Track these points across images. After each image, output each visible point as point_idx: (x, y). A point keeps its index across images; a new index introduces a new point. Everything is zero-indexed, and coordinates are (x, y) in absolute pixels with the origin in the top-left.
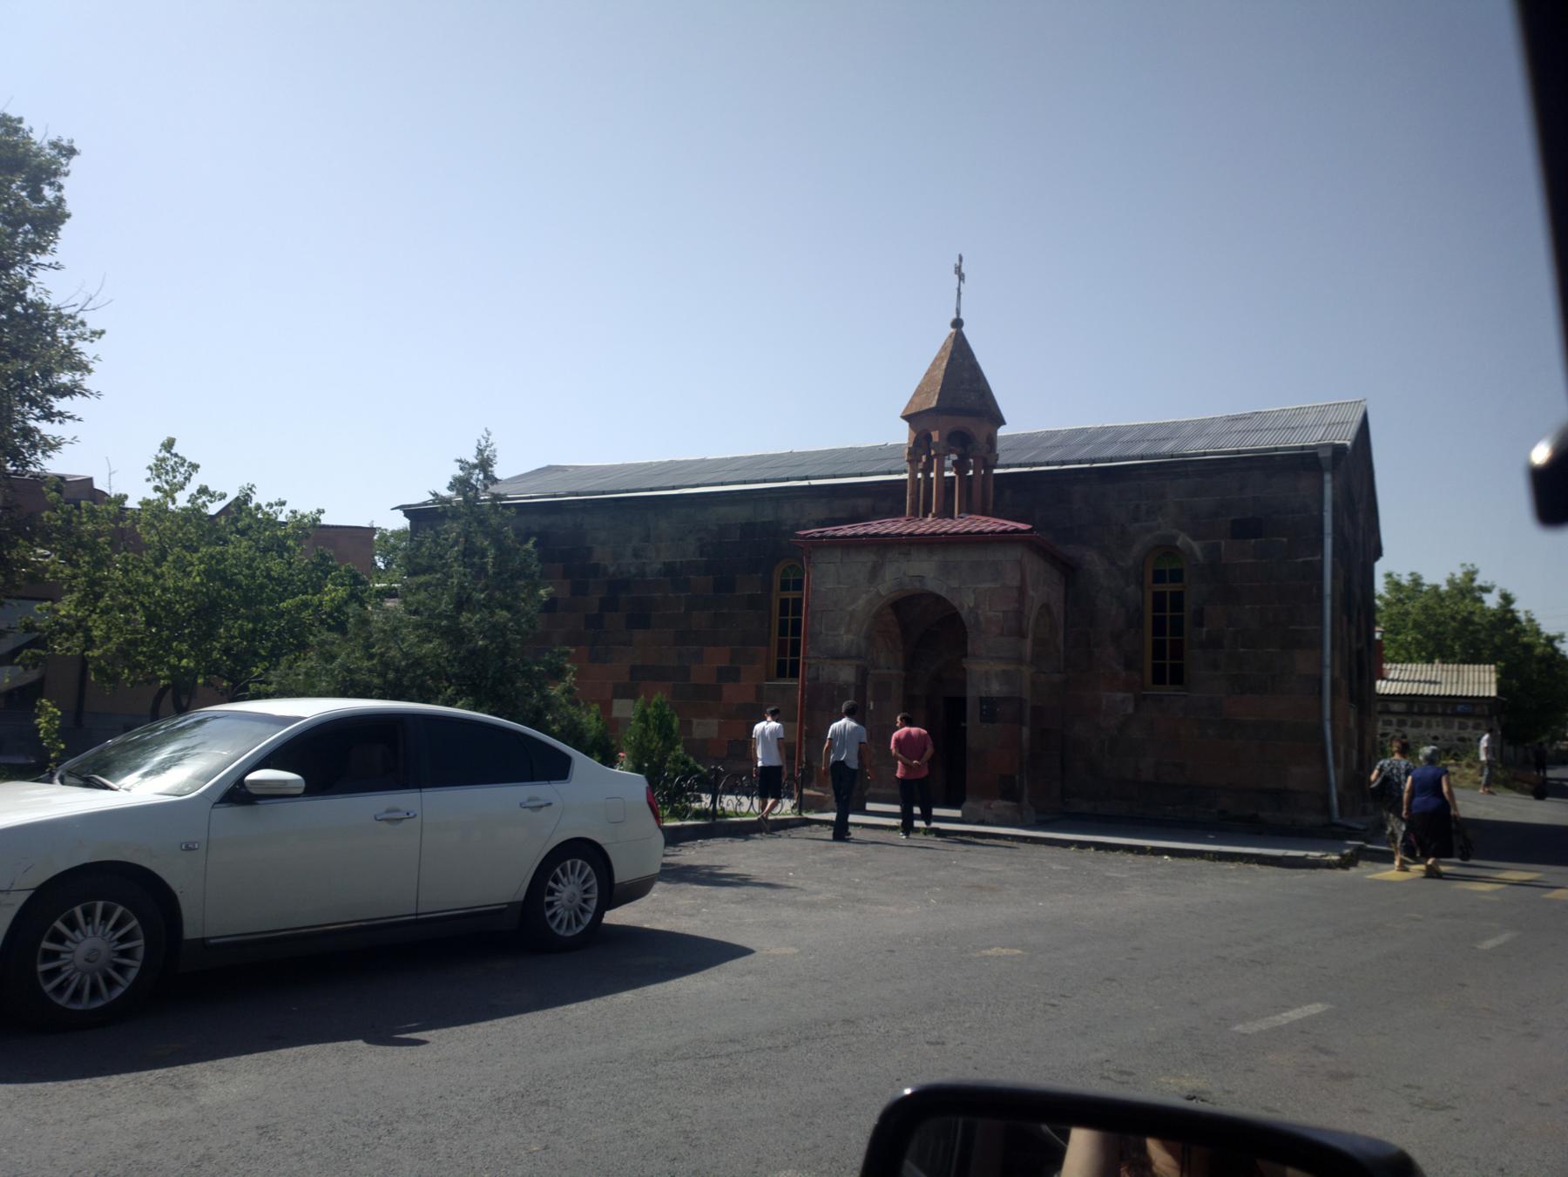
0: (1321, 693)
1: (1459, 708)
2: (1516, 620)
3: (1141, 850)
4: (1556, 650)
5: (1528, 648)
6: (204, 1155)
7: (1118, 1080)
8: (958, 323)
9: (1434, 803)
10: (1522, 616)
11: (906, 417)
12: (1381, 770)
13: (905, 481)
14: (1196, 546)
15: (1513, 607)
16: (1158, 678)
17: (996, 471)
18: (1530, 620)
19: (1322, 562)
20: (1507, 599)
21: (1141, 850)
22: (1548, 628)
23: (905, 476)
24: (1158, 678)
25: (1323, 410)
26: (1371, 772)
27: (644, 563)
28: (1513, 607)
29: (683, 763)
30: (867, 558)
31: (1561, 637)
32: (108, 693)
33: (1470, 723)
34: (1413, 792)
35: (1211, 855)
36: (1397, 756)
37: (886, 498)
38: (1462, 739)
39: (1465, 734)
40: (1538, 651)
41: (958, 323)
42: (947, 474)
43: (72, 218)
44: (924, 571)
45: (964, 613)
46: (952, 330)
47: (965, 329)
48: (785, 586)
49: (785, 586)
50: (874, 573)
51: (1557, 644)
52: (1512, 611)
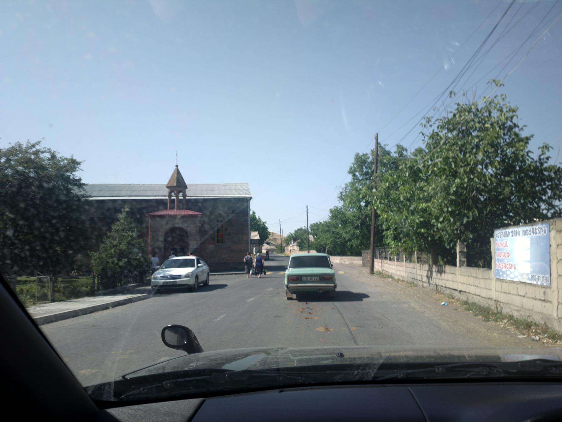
0: (248, 243)
1: (252, 242)
2: (256, 218)
3: (229, 274)
4: (265, 225)
6: (430, 214)
8: (177, 166)
10: (257, 217)
12: (246, 259)
13: (167, 199)
16: (218, 241)
17: (187, 198)
19: (248, 219)
21: (229, 274)
22: (263, 220)
23: (167, 198)
24: (218, 241)
25: (236, 185)
26: (244, 259)
28: (255, 215)
31: (266, 222)
32: (477, 256)
35: (80, 313)
36: (248, 255)
37: (160, 203)
40: (261, 226)
41: (177, 166)
42: (173, 198)
44: (179, 224)
46: (176, 167)
47: (179, 168)
51: (265, 224)
52: (255, 216)
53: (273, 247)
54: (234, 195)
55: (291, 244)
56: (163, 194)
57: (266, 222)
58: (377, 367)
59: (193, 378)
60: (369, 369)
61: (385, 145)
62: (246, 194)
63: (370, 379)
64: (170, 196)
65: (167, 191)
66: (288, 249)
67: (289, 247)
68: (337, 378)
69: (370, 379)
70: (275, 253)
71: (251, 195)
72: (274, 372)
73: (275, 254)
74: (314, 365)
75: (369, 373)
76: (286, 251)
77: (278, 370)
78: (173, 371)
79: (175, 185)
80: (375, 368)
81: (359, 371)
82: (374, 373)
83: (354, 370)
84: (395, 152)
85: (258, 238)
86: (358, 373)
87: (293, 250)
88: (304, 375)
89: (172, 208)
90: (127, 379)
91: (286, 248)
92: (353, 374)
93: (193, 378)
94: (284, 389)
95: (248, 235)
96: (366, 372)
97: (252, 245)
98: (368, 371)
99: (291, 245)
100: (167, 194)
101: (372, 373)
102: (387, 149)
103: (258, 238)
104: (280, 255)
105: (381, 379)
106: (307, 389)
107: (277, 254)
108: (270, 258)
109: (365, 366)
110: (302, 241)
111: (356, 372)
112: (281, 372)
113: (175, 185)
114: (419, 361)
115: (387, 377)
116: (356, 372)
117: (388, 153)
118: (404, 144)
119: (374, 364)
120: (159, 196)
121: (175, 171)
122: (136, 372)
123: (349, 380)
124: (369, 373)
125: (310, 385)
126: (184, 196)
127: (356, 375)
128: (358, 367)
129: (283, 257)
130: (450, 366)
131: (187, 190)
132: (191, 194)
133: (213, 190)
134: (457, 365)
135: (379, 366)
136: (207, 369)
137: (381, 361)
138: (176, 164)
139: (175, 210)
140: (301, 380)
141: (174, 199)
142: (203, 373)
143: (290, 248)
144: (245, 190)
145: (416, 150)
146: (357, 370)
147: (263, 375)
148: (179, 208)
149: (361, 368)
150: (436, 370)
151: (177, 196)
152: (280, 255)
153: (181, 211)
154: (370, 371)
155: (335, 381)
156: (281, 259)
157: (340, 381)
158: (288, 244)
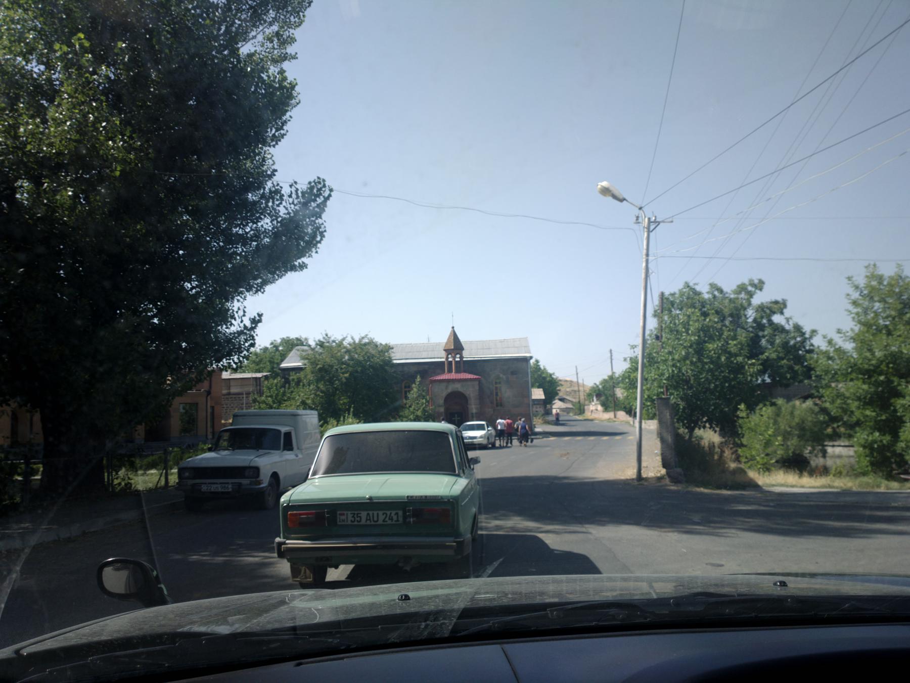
1: (536, 402)
2: (540, 369)
4: (553, 378)
5: (544, 378)
7: (647, 337)
8: (453, 328)
9: (525, 431)
11: (445, 350)
14: (504, 377)
15: (539, 364)
17: (464, 359)
18: (545, 369)
20: (537, 361)
22: (550, 371)
25: (514, 341)
27: (423, 409)
28: (539, 364)
29: (826, 374)
30: (444, 384)
33: (538, 406)
34: (521, 429)
37: (437, 367)
38: (537, 411)
39: (537, 410)
40: (548, 379)
41: (453, 328)
43: (264, 315)
44: (458, 387)
45: (467, 395)
48: (405, 387)
49: (405, 387)
50: (447, 387)
51: (553, 376)
52: (539, 366)
53: (569, 406)
54: (512, 354)
55: (593, 400)
56: (439, 356)
57: (554, 374)
58: (456, 614)
59: (141, 650)
60: (444, 619)
61: (695, 284)
62: (526, 353)
63: (446, 635)
64: (447, 358)
65: (444, 354)
66: (589, 409)
67: (591, 406)
68: (393, 637)
69: (446, 634)
70: (571, 414)
71: (530, 353)
72: (288, 633)
73: (572, 416)
74: (359, 617)
75: (444, 626)
76: (586, 412)
77: (294, 629)
78: (110, 638)
79: (453, 348)
80: (454, 617)
81: (428, 622)
82: (453, 624)
83: (420, 622)
84: (708, 293)
85: (543, 397)
86: (427, 626)
87: (596, 411)
88: (338, 636)
89: (450, 371)
90: (22, 655)
91: (586, 407)
92: (419, 627)
93: (141, 650)
94: (303, 661)
95: (529, 394)
96: (439, 623)
97: (535, 406)
98: (442, 622)
99: (593, 403)
100: (445, 356)
101: (448, 625)
102: (698, 288)
103: (543, 397)
104: (577, 417)
105: (463, 633)
106: (342, 659)
107: (574, 417)
108: (561, 422)
109: (437, 614)
110: (607, 398)
111: (423, 625)
112: (298, 632)
113: (453, 348)
114: (524, 601)
115: (474, 629)
116: (423, 625)
117: (699, 294)
118: (664, 291)
119: (452, 611)
120: (434, 358)
121: (451, 333)
122: (43, 643)
123: (412, 639)
124: (444, 626)
125: (348, 650)
126: (461, 357)
127: (423, 629)
128: (426, 616)
129: (581, 420)
130: (570, 606)
131: (464, 352)
132: (468, 355)
133: (489, 349)
134: (579, 605)
135: (459, 613)
136: (165, 634)
137: (462, 606)
138: (452, 326)
139: (453, 373)
140: (333, 641)
141: (451, 362)
142: (158, 641)
143: (592, 407)
144: (525, 347)
145: (738, 286)
146: (425, 621)
147: (265, 638)
148: (458, 371)
149: (432, 618)
150: (550, 615)
151: (454, 358)
152: (577, 417)
153: (459, 374)
154: (446, 621)
155: (390, 641)
156: (571, 423)
157: (398, 641)
158: (591, 401)
